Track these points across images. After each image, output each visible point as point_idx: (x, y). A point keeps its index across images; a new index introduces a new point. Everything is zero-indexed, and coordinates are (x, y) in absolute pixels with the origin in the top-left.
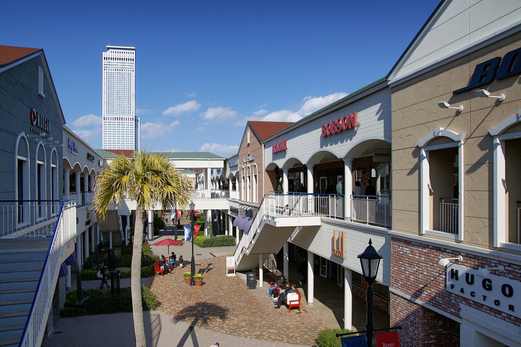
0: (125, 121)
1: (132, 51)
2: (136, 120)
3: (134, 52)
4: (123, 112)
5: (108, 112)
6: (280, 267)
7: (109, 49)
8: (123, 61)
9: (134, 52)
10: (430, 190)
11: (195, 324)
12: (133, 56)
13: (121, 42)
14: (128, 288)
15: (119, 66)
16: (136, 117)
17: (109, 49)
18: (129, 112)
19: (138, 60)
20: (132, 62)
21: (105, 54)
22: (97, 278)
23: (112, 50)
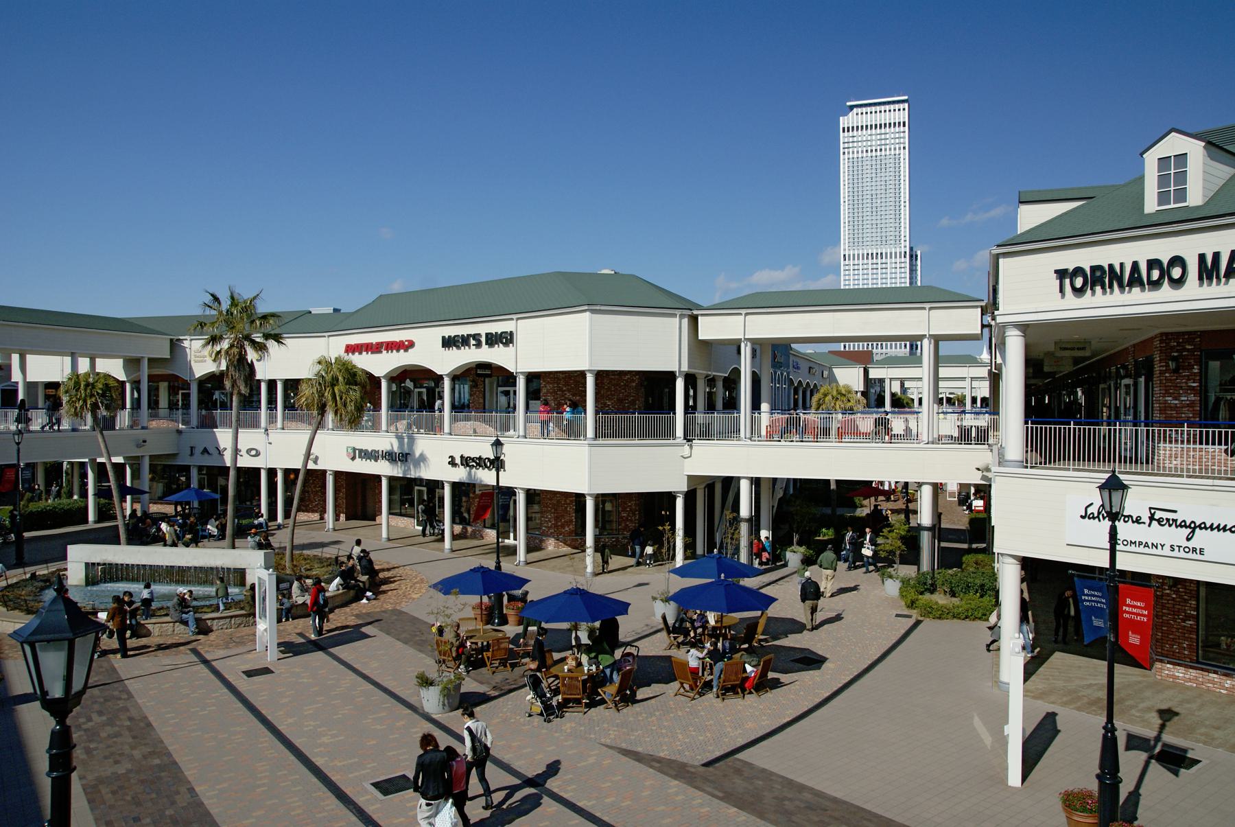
0: (889, 260)
1: (901, 106)
2: (911, 256)
3: (906, 105)
4: (884, 241)
5: (853, 243)
6: (910, 617)
7: (852, 108)
8: (883, 131)
9: (906, 105)
10: (1022, 591)
11: (367, 351)
12: (904, 116)
13: (874, 88)
14: (79, 509)
15: (875, 139)
16: (911, 249)
17: (852, 108)
18: (897, 240)
19: (914, 124)
20: (902, 129)
21: (844, 122)
22: (979, 364)
23: (860, 110)
